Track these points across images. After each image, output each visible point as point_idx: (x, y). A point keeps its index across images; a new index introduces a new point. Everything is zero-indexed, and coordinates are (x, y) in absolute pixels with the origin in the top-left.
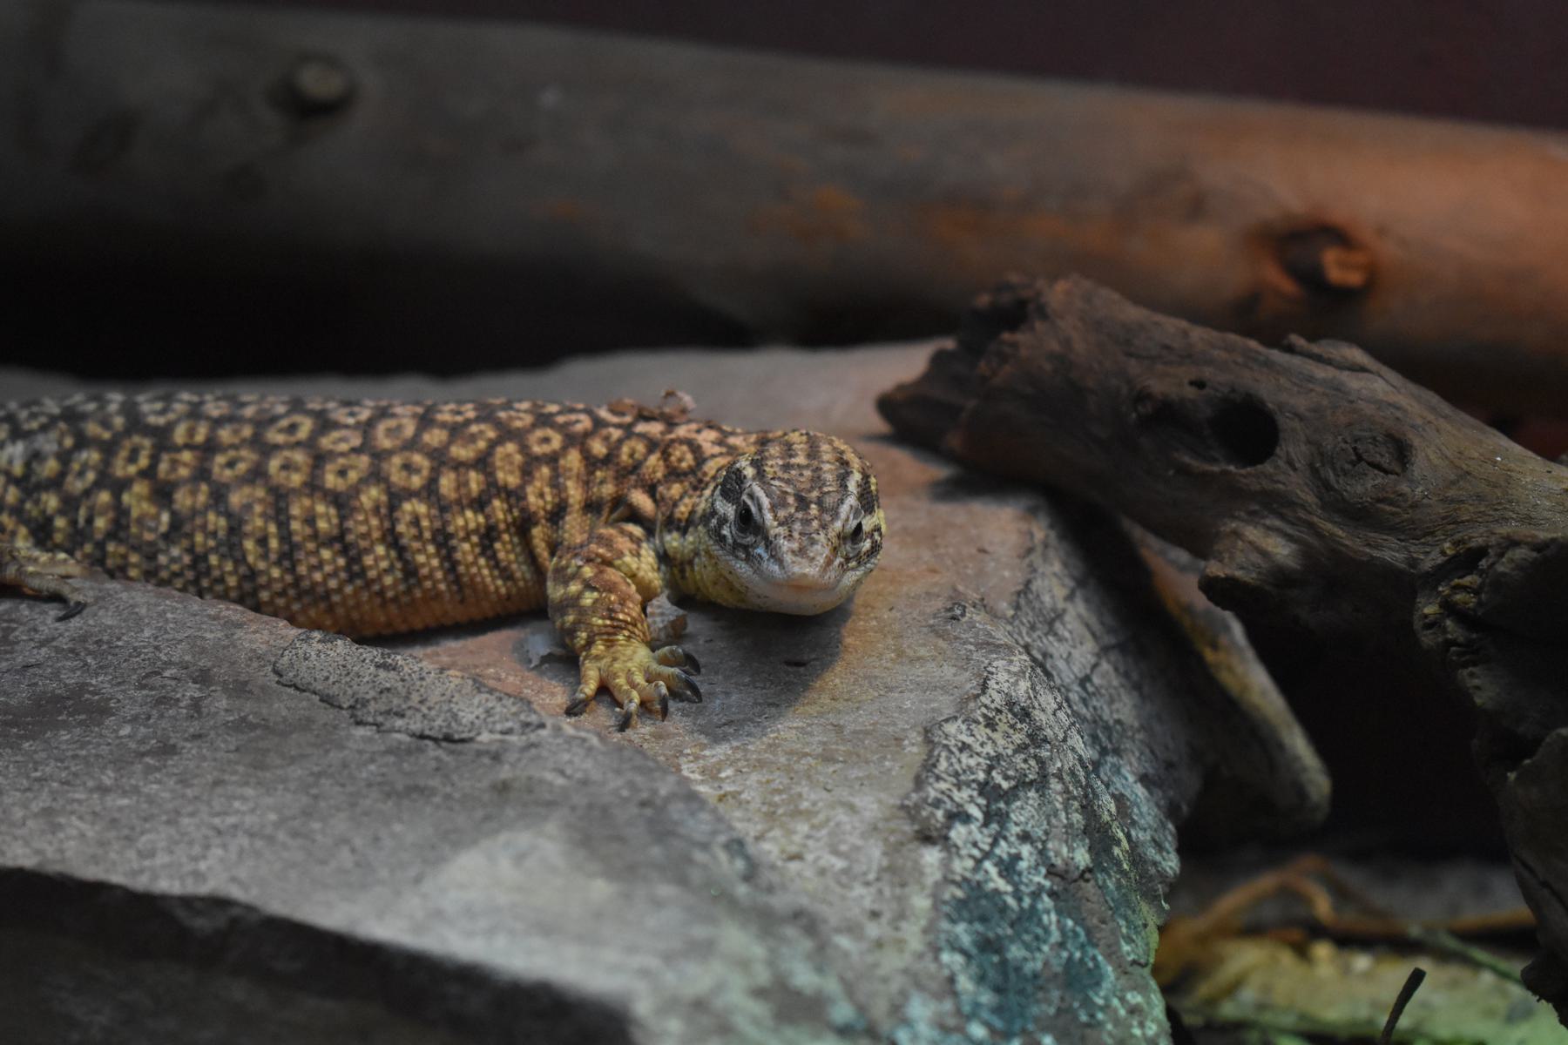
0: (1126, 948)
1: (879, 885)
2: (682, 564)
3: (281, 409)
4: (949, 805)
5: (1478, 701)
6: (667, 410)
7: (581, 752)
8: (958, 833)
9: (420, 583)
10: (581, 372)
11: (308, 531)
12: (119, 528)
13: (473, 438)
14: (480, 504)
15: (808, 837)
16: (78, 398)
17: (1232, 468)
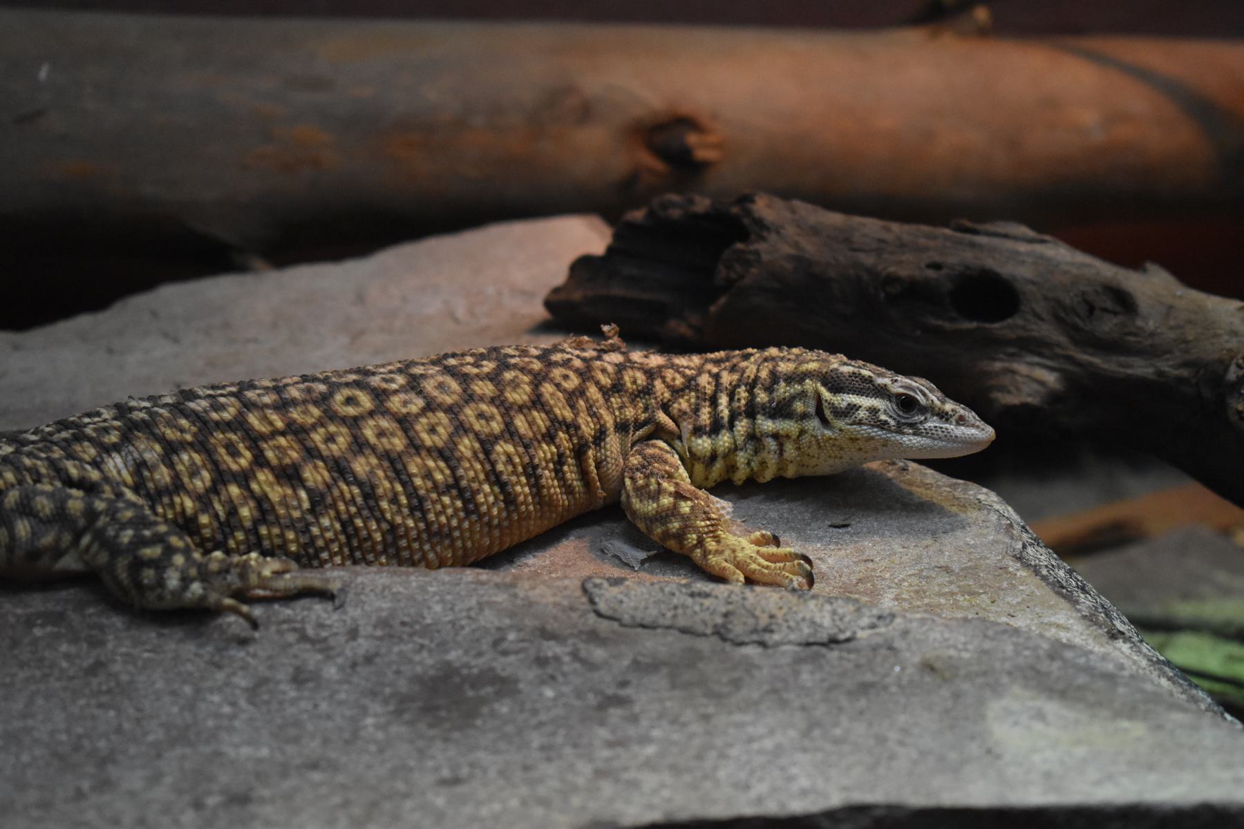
14: (550, 437)
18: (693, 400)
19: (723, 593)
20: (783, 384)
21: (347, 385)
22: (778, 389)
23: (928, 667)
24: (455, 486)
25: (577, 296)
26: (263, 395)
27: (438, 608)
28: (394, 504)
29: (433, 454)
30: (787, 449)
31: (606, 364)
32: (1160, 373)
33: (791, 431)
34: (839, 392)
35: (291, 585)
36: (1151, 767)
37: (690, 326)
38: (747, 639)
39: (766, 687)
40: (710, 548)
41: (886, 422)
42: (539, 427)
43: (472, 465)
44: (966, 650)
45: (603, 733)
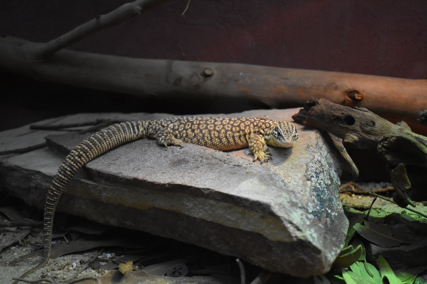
0: (336, 195)
1: (302, 187)
2: (268, 140)
3: (209, 119)
4: (311, 175)
5: (388, 160)
6: (265, 118)
7: (258, 168)
8: (312, 179)
9: (230, 143)
10: (246, 113)
11: (214, 136)
12: (187, 136)
13: (237, 123)
14: (239, 132)
15: (291, 180)
16: (180, 117)
17: (348, 126)
32: (376, 139)
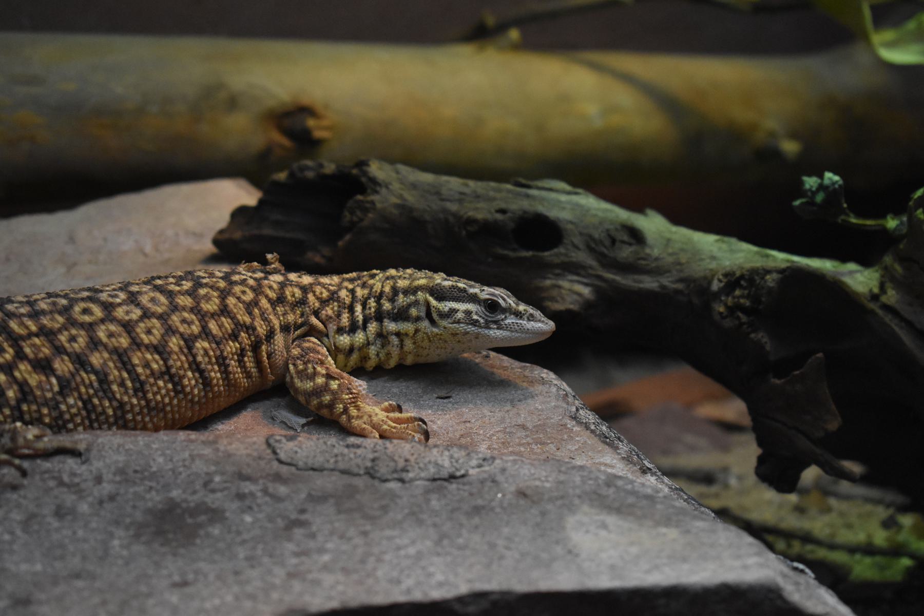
14: (234, 336)
18: (336, 308)
19: (369, 444)
20: (401, 296)
21: (83, 299)
22: (398, 300)
23: (522, 494)
24: (167, 373)
25: (237, 235)
26: (20, 307)
27: (161, 460)
28: (121, 387)
29: (150, 349)
30: (407, 344)
31: (272, 283)
32: (663, 287)
33: (409, 330)
34: (443, 301)
35: (49, 446)
36: (684, 560)
37: (323, 256)
38: (389, 477)
39: (406, 511)
40: (353, 414)
41: (477, 321)
42: (226, 329)
43: (179, 358)
44: (547, 481)
45: (291, 546)
